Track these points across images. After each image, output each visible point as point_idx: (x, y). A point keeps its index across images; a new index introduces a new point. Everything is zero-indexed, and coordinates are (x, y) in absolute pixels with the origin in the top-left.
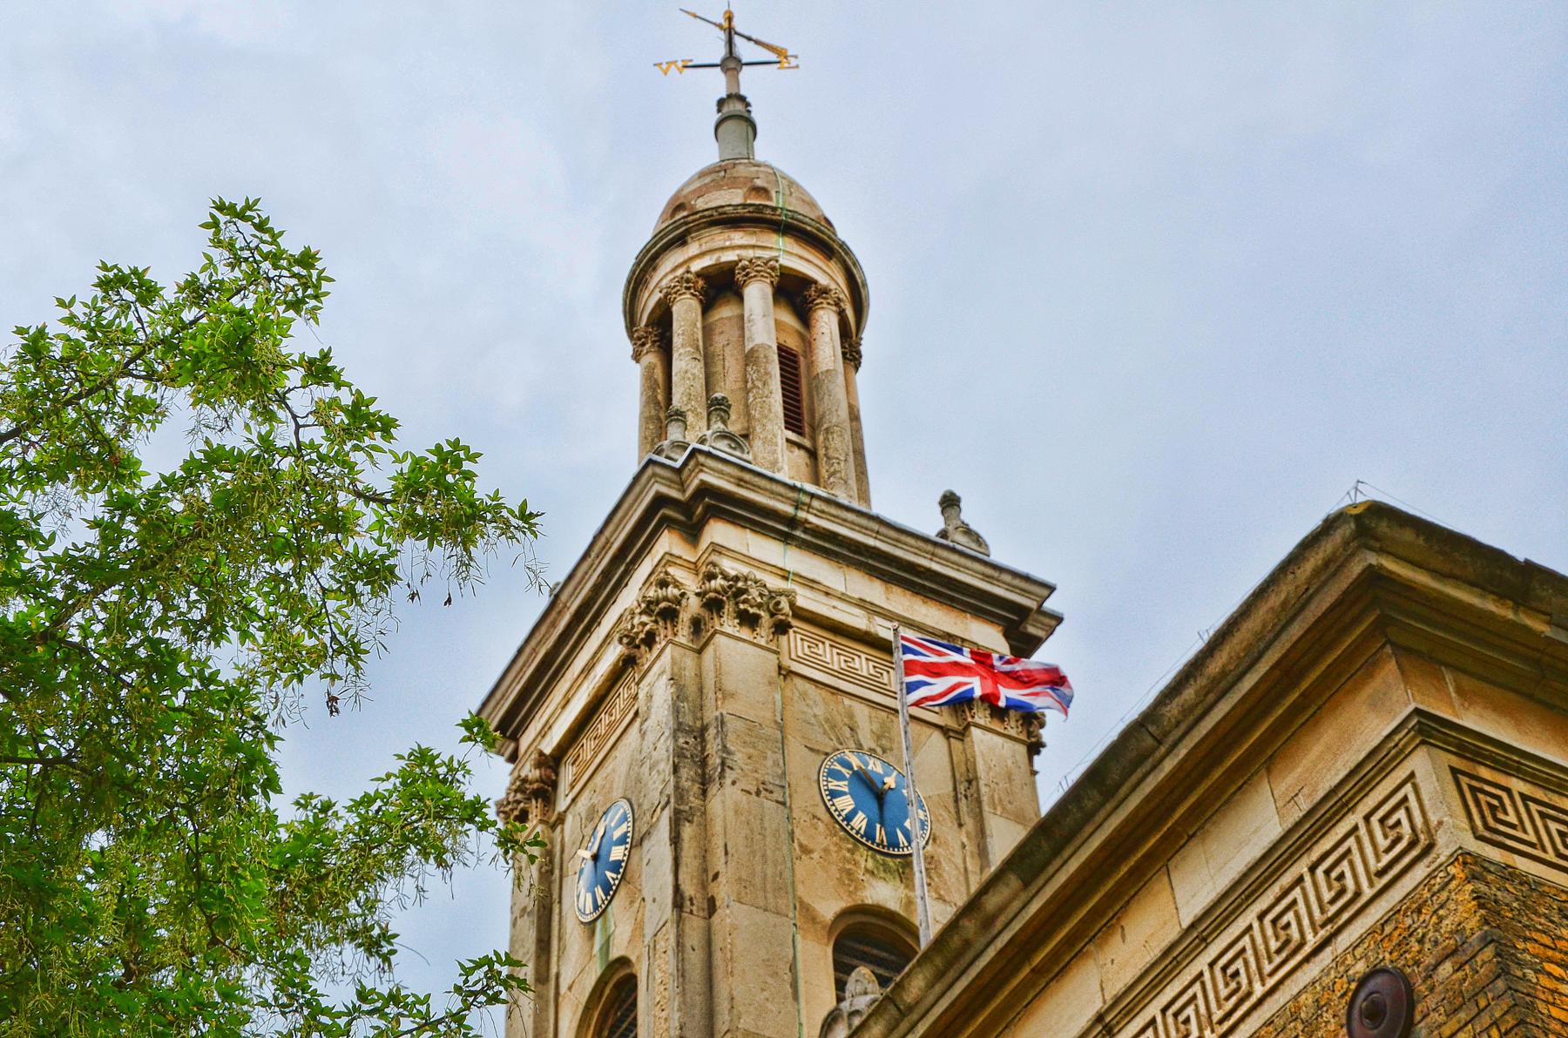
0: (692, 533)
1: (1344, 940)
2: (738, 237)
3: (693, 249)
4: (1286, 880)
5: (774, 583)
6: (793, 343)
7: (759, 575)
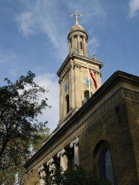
0: (73, 60)
1: (116, 103)
2: (77, 32)
3: (73, 33)
4: (112, 98)
5: (79, 64)
6: (82, 41)
7: (78, 63)
